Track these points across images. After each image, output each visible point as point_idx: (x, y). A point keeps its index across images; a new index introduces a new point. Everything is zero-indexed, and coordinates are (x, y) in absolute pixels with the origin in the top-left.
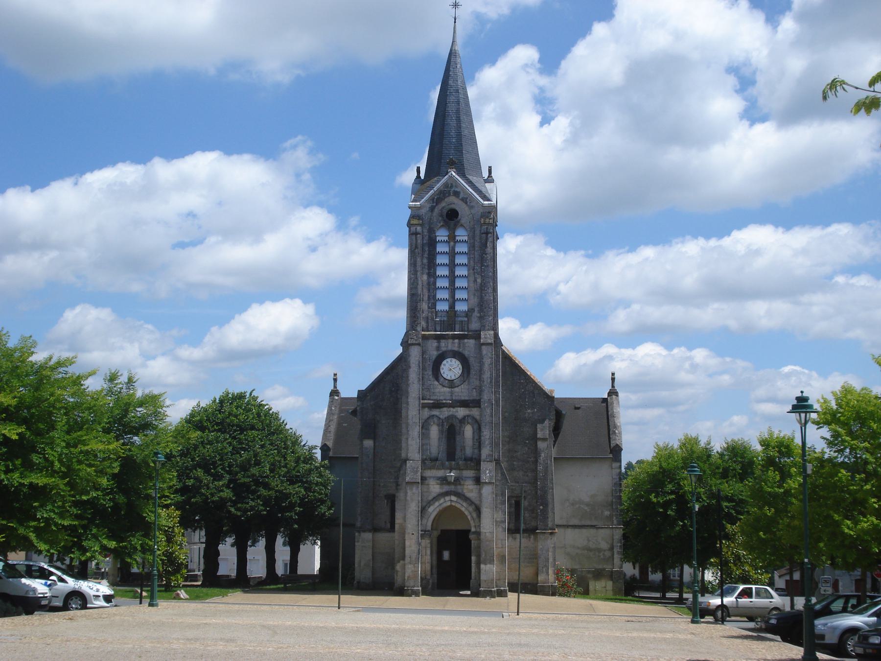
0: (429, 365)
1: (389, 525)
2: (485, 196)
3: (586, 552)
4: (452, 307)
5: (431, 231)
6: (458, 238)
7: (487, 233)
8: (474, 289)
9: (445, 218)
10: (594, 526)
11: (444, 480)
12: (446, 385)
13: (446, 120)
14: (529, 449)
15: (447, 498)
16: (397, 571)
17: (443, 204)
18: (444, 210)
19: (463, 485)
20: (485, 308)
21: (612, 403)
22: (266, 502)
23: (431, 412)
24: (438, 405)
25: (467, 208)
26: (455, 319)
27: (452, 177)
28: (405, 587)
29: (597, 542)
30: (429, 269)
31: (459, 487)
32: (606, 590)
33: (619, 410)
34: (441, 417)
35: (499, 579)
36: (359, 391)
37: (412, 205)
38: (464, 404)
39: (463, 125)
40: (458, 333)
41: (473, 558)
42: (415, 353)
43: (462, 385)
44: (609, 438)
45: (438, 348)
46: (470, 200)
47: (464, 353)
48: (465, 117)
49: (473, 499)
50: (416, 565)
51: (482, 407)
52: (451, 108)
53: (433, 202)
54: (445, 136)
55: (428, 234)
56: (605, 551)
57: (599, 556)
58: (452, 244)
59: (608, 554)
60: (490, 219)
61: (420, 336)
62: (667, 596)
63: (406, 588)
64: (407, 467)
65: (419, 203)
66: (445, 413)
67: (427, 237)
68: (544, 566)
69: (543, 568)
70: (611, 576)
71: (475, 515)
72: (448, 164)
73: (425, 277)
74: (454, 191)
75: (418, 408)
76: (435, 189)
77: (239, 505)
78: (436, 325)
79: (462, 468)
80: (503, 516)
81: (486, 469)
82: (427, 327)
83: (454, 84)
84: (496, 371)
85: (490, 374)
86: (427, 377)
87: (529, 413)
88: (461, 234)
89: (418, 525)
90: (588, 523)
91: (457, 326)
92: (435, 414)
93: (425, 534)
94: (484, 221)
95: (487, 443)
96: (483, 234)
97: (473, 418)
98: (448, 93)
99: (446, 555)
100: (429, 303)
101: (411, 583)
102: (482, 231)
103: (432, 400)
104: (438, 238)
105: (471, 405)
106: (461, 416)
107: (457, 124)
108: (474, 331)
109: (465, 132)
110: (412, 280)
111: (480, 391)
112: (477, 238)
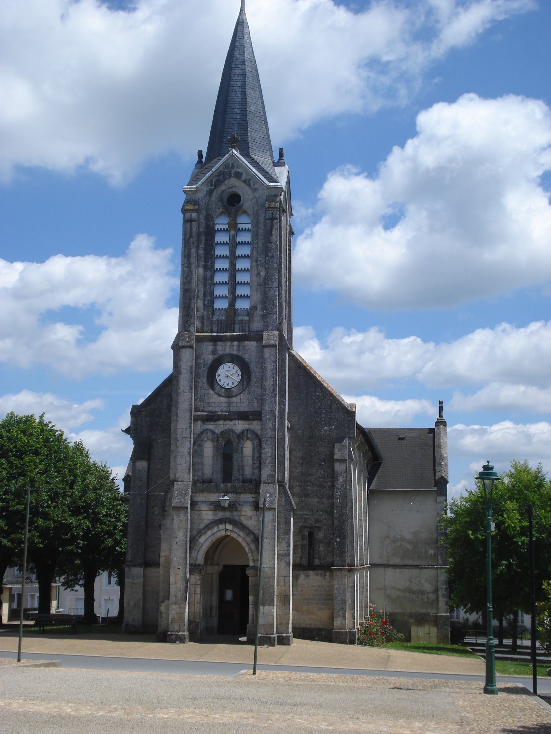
0: (204, 371)
2: (271, 177)
3: (408, 594)
4: (232, 304)
5: (209, 218)
6: (240, 226)
7: (272, 219)
8: (256, 284)
9: (226, 203)
10: (417, 566)
11: (217, 506)
12: (223, 394)
13: (229, 95)
14: (325, 471)
15: (222, 527)
16: (161, 613)
17: (223, 187)
18: (224, 195)
19: (240, 511)
20: (269, 305)
21: (439, 434)
22: (44, 533)
23: (206, 426)
24: (212, 418)
25: (250, 192)
26: (235, 318)
27: (232, 155)
28: (168, 631)
30: (206, 260)
31: (235, 513)
32: (430, 637)
33: (446, 440)
34: (216, 431)
35: (281, 624)
36: (133, 406)
37: (187, 188)
38: (243, 416)
39: (249, 100)
40: (237, 334)
41: (251, 598)
42: (187, 355)
43: (242, 395)
44: (435, 470)
45: (214, 352)
46: (253, 182)
47: (244, 357)
48: (252, 92)
49: (252, 528)
50: (182, 605)
51: (264, 419)
52: (236, 82)
53: (211, 185)
54: (228, 112)
55: (205, 221)
56: (428, 593)
57: (422, 599)
58: (233, 232)
59: (432, 597)
60: (276, 202)
61: (193, 337)
62: (504, 643)
63: (169, 633)
65: (194, 186)
66: (221, 426)
67: (204, 225)
68: (341, 608)
69: (339, 611)
70: (436, 621)
71: (253, 547)
72: (229, 141)
73: (201, 271)
74: (235, 172)
75: (189, 421)
76: (214, 170)
77: (13, 536)
78: (212, 325)
79: (239, 491)
80: (286, 549)
81: (267, 492)
84: (281, 378)
85: (273, 381)
86: (200, 385)
87: (325, 431)
88: (244, 222)
89: (186, 558)
90: (411, 562)
91: (237, 327)
92: (209, 428)
93: (194, 568)
94: (270, 205)
95: (268, 461)
96: (267, 219)
97: (254, 433)
98: (233, 66)
100: (204, 300)
101: (176, 627)
102: (267, 217)
103: (207, 412)
104: (217, 227)
105: (251, 417)
107: (242, 99)
108: (256, 332)
109: (252, 108)
110: (186, 273)
111: (261, 400)
112: (261, 226)
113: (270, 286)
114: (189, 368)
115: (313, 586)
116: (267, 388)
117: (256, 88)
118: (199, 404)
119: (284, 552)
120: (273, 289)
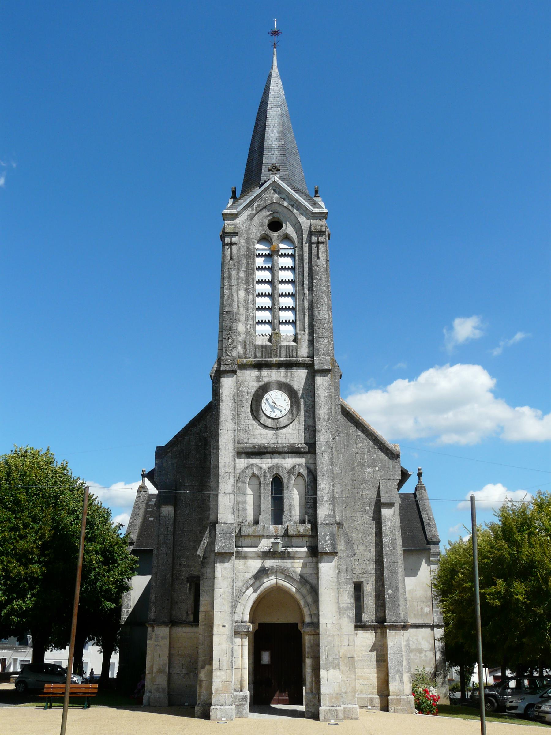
1: (191, 618)
16: (201, 681)
29: (417, 641)
36: (158, 447)
41: (308, 662)
43: (291, 425)
44: (424, 531)
45: (258, 379)
47: (292, 384)
56: (426, 651)
64: (217, 532)
67: (245, 248)
71: (310, 599)
73: (242, 294)
82: (245, 353)
83: (275, 101)
95: (325, 499)
99: (266, 658)
100: (246, 325)
106: (289, 466)
113: (319, 309)
114: (231, 395)
115: (362, 646)
116: (322, 417)
117: (291, 131)
118: (243, 435)
119: (346, 605)
120: (323, 312)
